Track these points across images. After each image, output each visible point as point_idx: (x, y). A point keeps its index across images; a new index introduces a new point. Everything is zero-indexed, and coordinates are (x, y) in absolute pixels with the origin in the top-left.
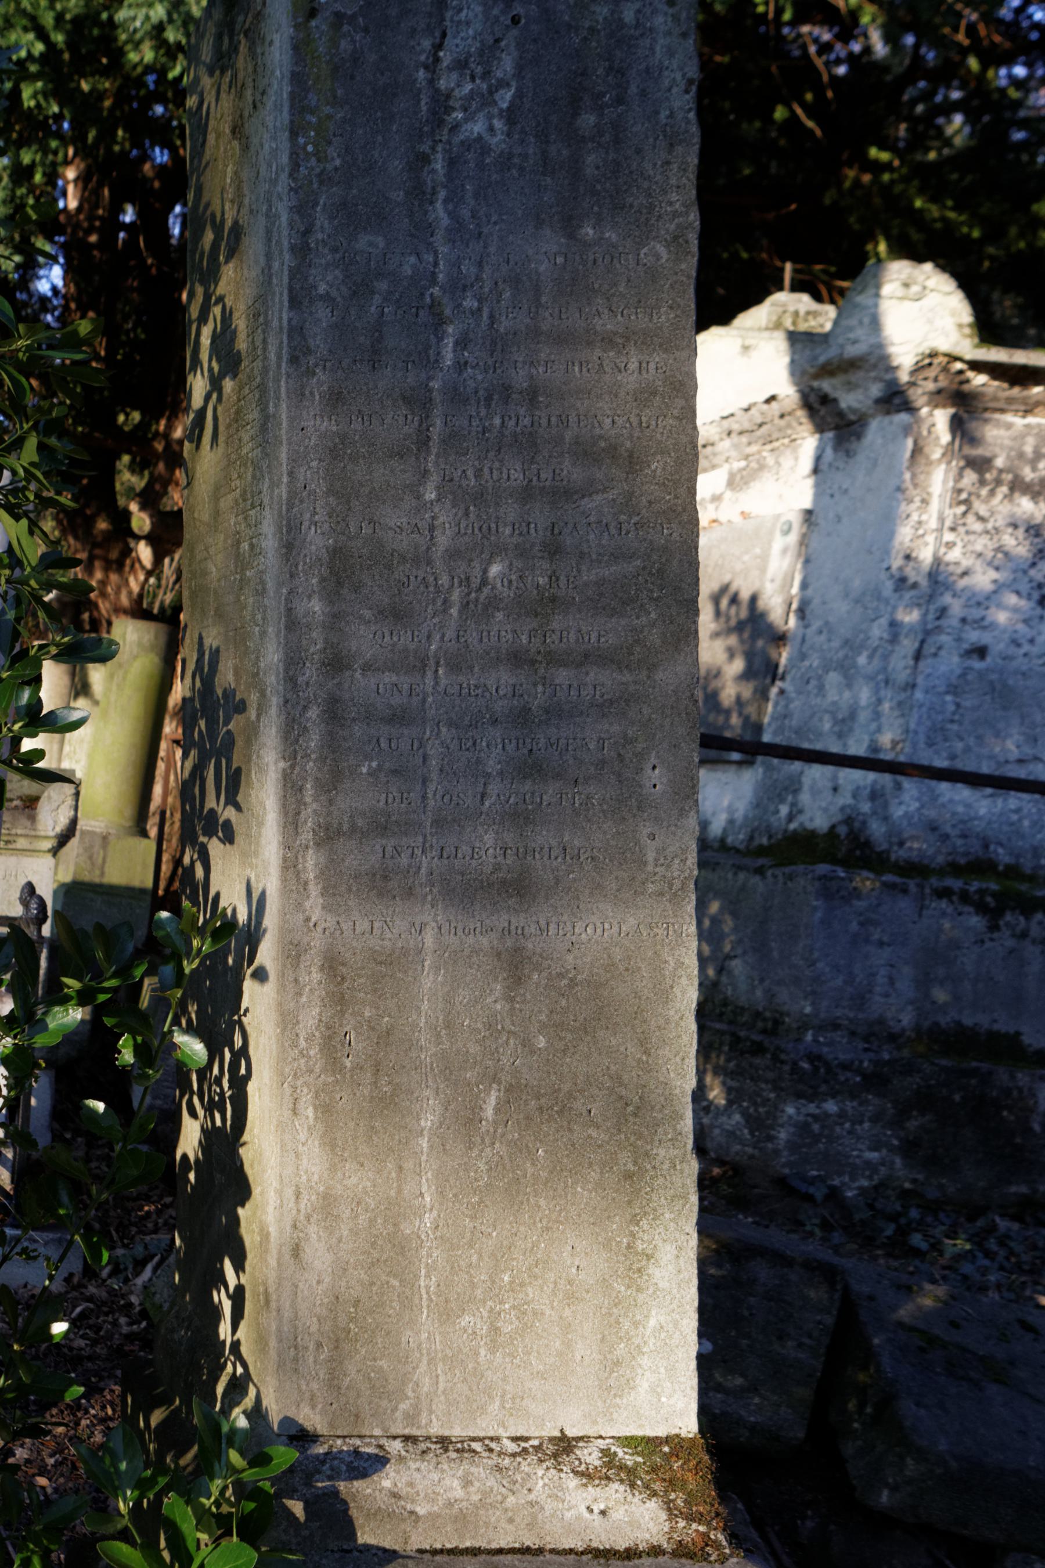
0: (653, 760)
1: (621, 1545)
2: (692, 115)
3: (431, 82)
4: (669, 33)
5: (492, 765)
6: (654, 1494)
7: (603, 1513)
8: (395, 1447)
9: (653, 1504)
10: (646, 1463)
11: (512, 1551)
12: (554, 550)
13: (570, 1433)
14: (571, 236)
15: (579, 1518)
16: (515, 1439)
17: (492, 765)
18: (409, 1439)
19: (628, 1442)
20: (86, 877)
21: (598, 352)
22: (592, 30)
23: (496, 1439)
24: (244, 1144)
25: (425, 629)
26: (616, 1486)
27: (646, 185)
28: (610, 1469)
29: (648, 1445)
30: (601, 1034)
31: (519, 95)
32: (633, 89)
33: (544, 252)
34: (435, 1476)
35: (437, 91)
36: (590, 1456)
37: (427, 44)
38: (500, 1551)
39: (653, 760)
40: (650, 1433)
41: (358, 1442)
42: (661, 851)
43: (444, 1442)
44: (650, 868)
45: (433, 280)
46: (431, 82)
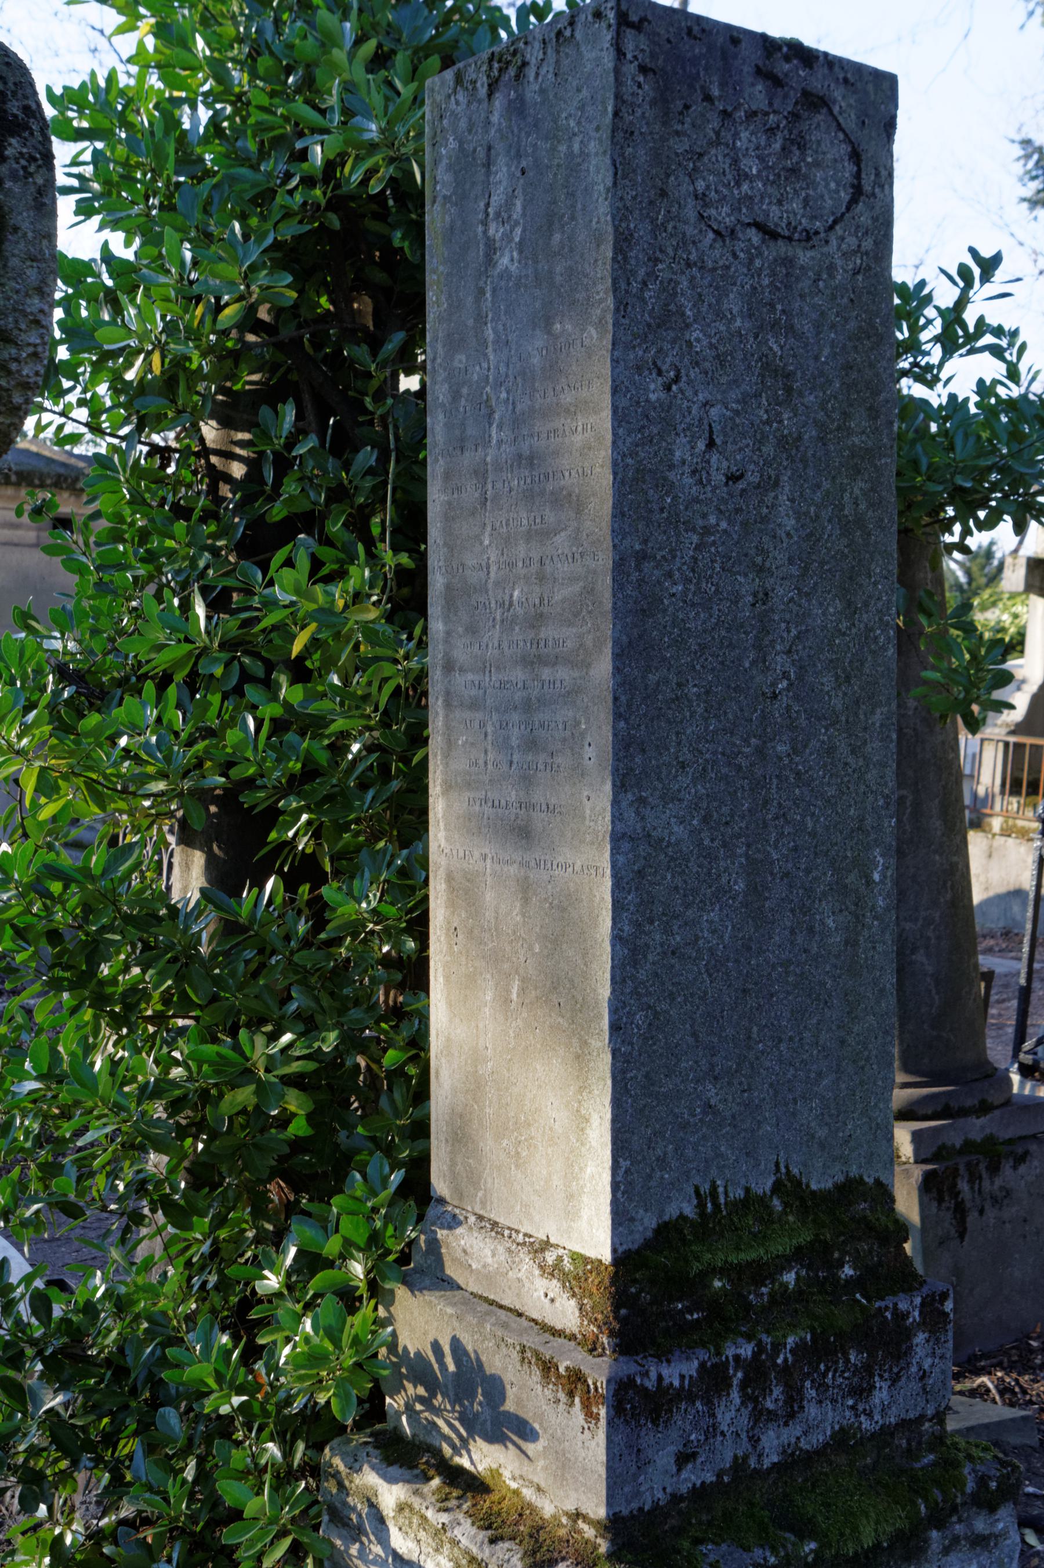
0: (589, 739)
1: (559, 1327)
2: (609, 218)
3: (485, 232)
4: (596, 154)
5: (514, 742)
6: (574, 1295)
7: (552, 1300)
8: (472, 1219)
9: (573, 1302)
10: (574, 1274)
11: (510, 1310)
12: (541, 578)
13: (552, 1240)
14: (549, 333)
15: (539, 1298)
16: (525, 1235)
17: (514, 742)
18: (480, 1218)
19: (575, 1257)
20: (189, 850)
21: (562, 421)
22: (558, 165)
23: (517, 1232)
24: (415, 994)
25: (485, 640)
26: (555, 1281)
27: (585, 281)
28: (554, 1271)
29: (578, 1258)
30: (564, 946)
31: (524, 231)
32: (579, 206)
33: (535, 348)
34: (482, 1245)
35: (488, 238)
36: (550, 1257)
37: (482, 204)
38: (501, 1307)
39: (589, 739)
40: (588, 1254)
41: (457, 1211)
42: (592, 809)
43: (495, 1224)
44: (587, 823)
45: (487, 382)
46: (485, 232)
